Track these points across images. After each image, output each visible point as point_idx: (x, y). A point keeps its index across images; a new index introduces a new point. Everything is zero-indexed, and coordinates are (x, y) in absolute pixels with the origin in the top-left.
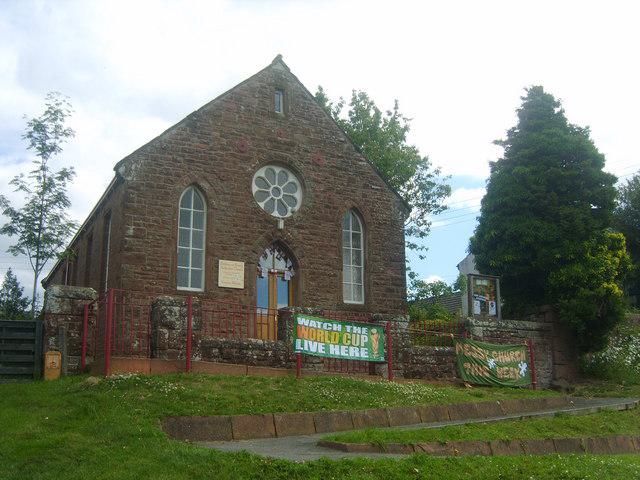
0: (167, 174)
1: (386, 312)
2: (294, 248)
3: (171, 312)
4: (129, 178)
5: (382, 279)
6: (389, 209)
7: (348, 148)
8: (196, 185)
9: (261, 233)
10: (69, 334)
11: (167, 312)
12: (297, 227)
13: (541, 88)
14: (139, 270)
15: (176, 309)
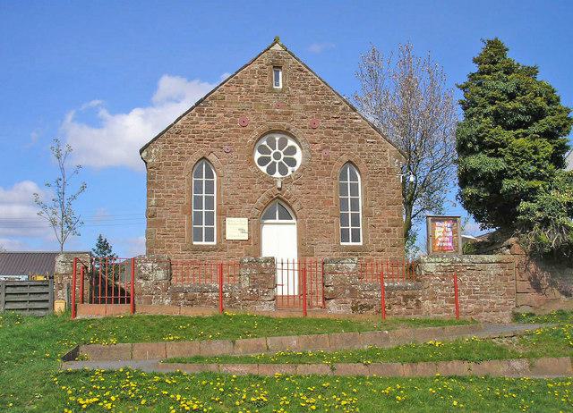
3: (145, 268)
4: (150, 161)
5: (378, 221)
7: (344, 109)
11: (142, 268)
15: (150, 265)
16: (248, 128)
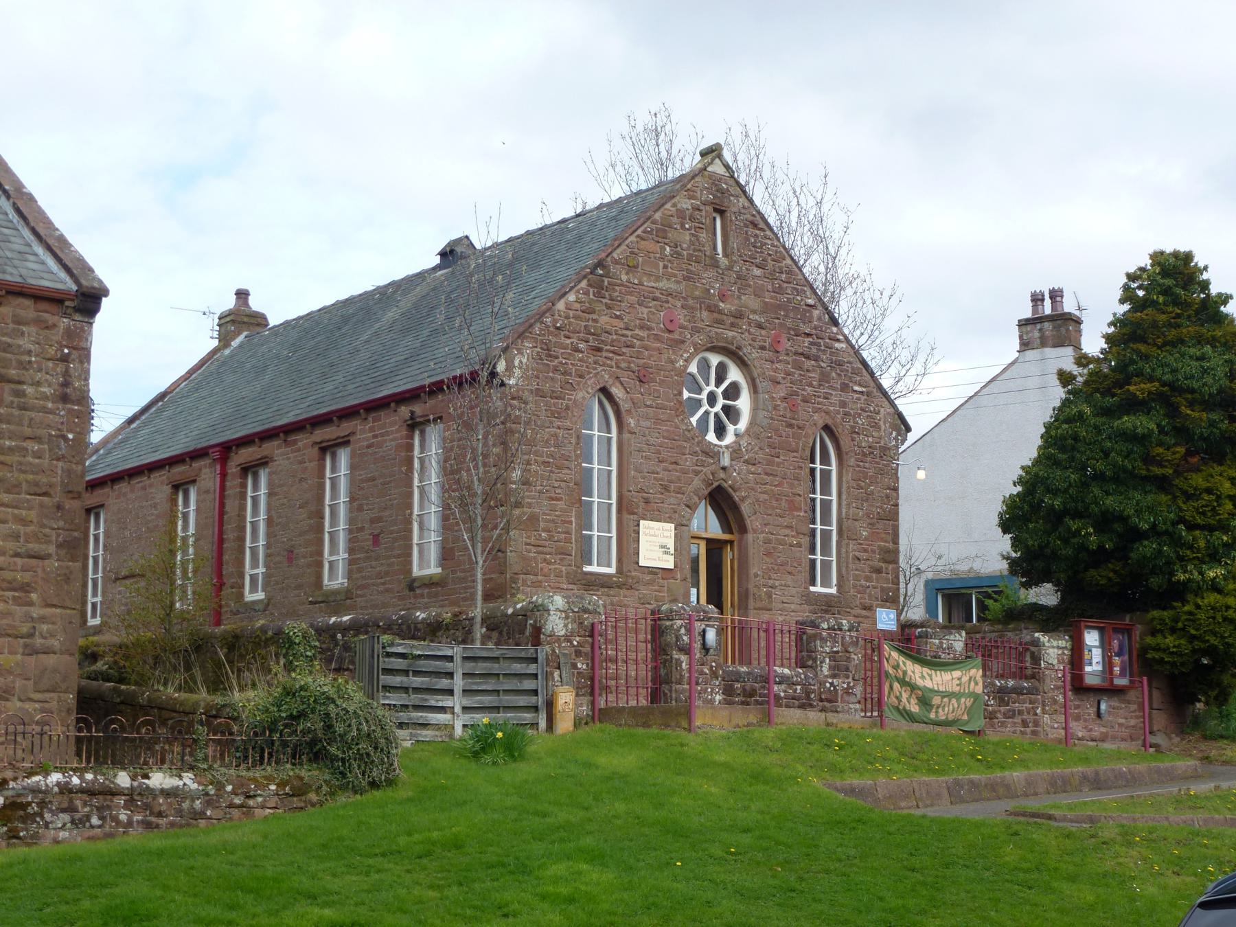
0: (565, 373)
1: (369, 447)
2: (743, 499)
6: (876, 426)
8: (604, 391)
9: (697, 473)
10: (574, 666)
12: (747, 462)
13: (1188, 257)
14: (532, 541)
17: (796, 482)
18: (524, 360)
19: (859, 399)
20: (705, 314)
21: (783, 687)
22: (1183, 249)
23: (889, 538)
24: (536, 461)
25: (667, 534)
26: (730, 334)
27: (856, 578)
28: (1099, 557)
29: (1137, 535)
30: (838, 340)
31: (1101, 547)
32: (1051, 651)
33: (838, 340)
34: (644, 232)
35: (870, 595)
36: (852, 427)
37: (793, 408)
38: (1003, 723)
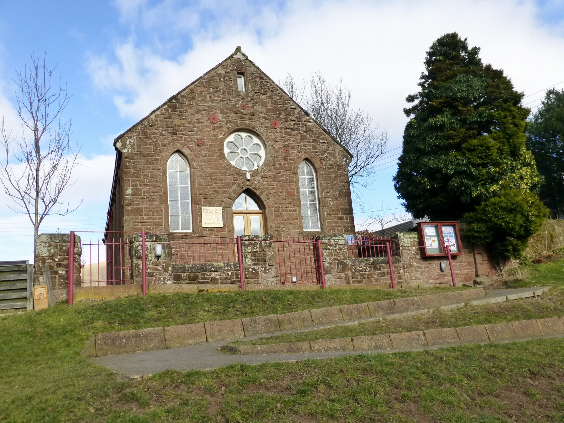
0: (155, 145)
2: (261, 193)
6: (334, 156)
7: (299, 114)
12: (261, 177)
14: (139, 220)
16: (217, 125)
17: (291, 184)
18: (132, 141)
19: (323, 145)
20: (233, 115)
21: (219, 273)
22: (451, 32)
23: (347, 204)
24: (140, 185)
25: (218, 212)
26: (247, 122)
27: (329, 223)
28: (434, 192)
29: (447, 178)
30: (310, 122)
31: (433, 188)
32: (405, 240)
33: (310, 122)
34: (198, 83)
35: (338, 230)
36: (320, 158)
37: (287, 152)
38: (377, 280)
